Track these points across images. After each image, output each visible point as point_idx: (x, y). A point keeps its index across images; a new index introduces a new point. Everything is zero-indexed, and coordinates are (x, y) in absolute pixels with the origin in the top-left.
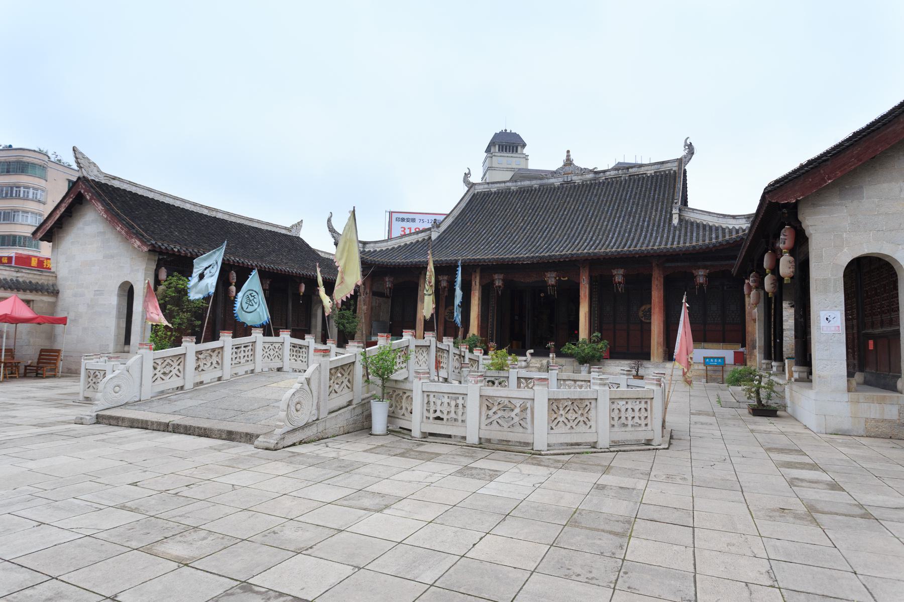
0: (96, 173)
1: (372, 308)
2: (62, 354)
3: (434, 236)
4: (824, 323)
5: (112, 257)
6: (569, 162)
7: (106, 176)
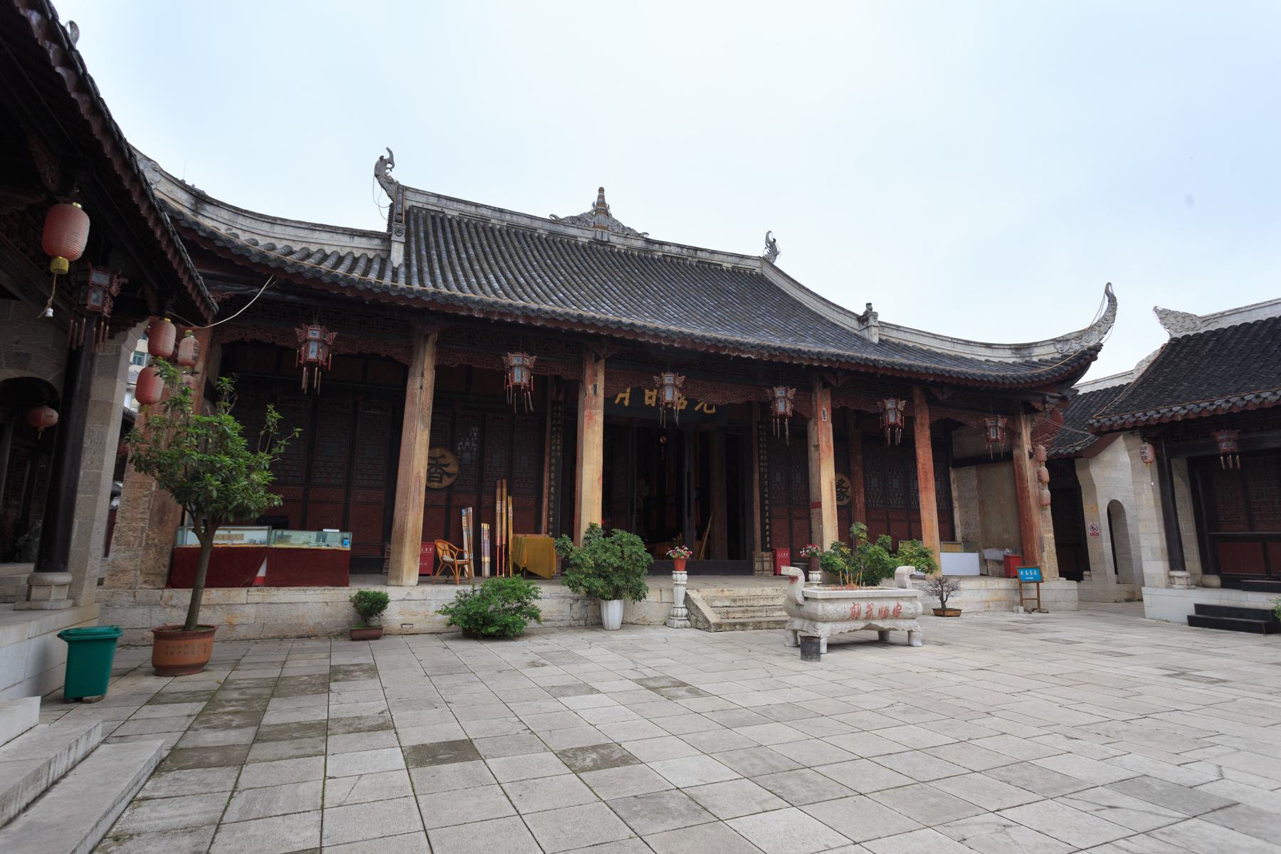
6: (601, 207)
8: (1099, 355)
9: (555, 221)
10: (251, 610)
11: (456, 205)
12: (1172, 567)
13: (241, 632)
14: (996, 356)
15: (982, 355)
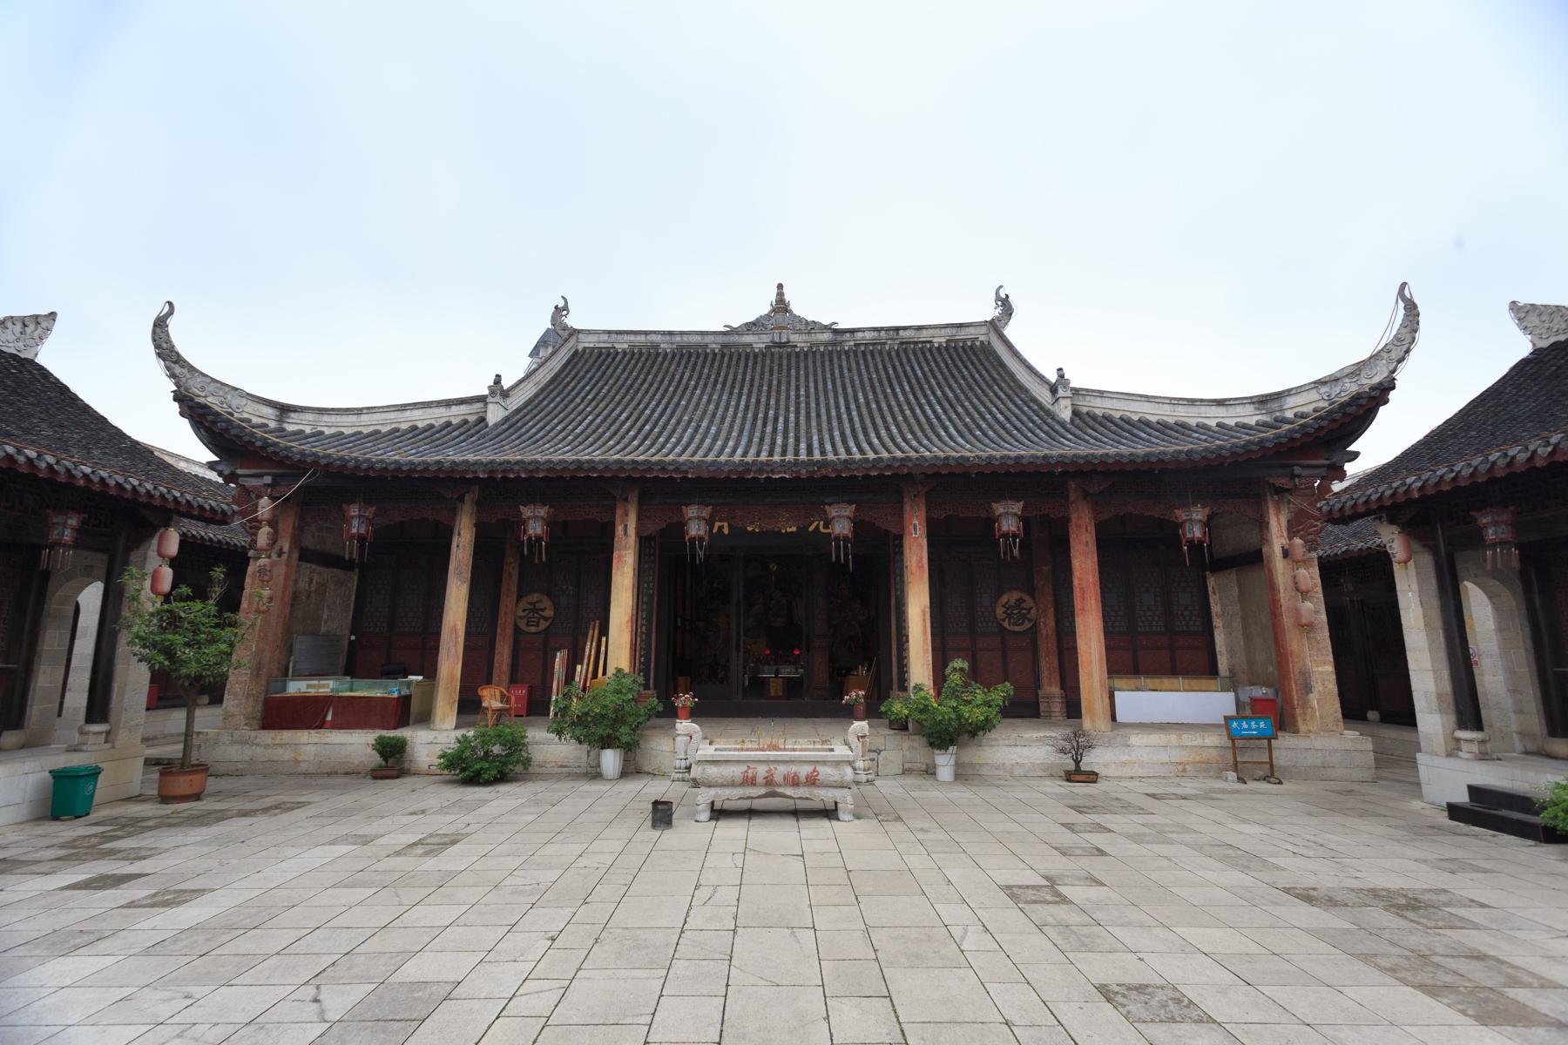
1: (295, 597)
3: (494, 415)
6: (781, 306)
8: (1392, 395)
9: (733, 331)
10: (311, 749)
11: (626, 338)
12: (1462, 724)
13: (304, 767)
14: (1230, 417)
15: (1212, 417)
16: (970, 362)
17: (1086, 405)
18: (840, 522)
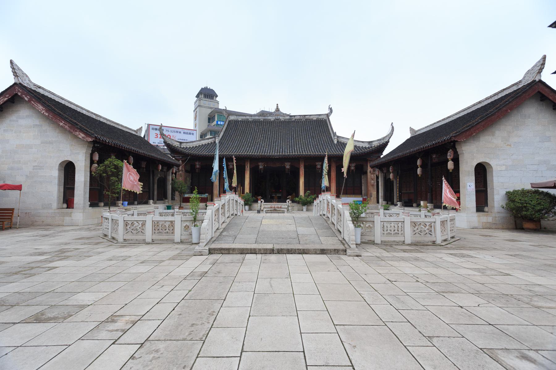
0: (28, 82)
2: (15, 212)
4: (468, 187)
5: (51, 143)
6: (278, 109)
7: (35, 85)
16: (320, 126)
17: (341, 140)
18: (288, 166)
